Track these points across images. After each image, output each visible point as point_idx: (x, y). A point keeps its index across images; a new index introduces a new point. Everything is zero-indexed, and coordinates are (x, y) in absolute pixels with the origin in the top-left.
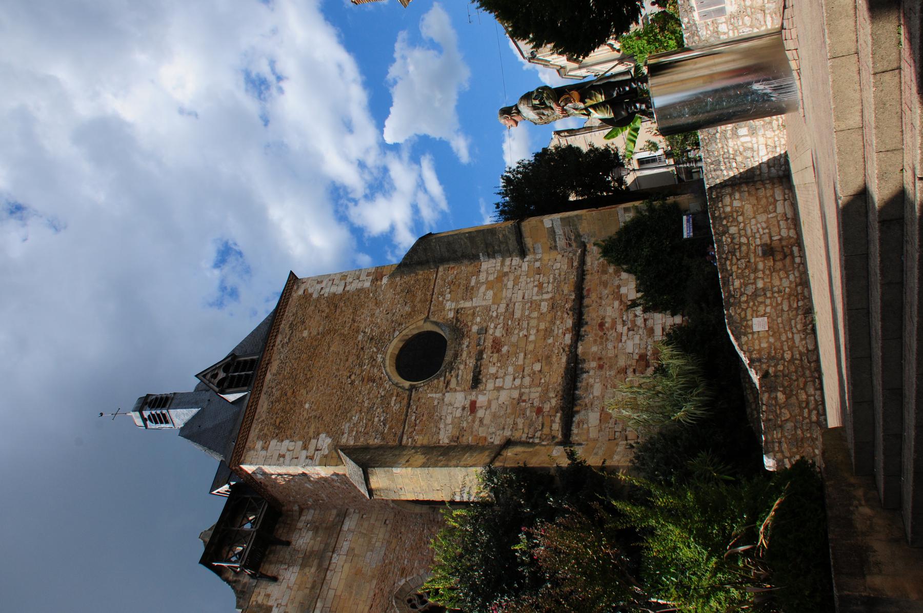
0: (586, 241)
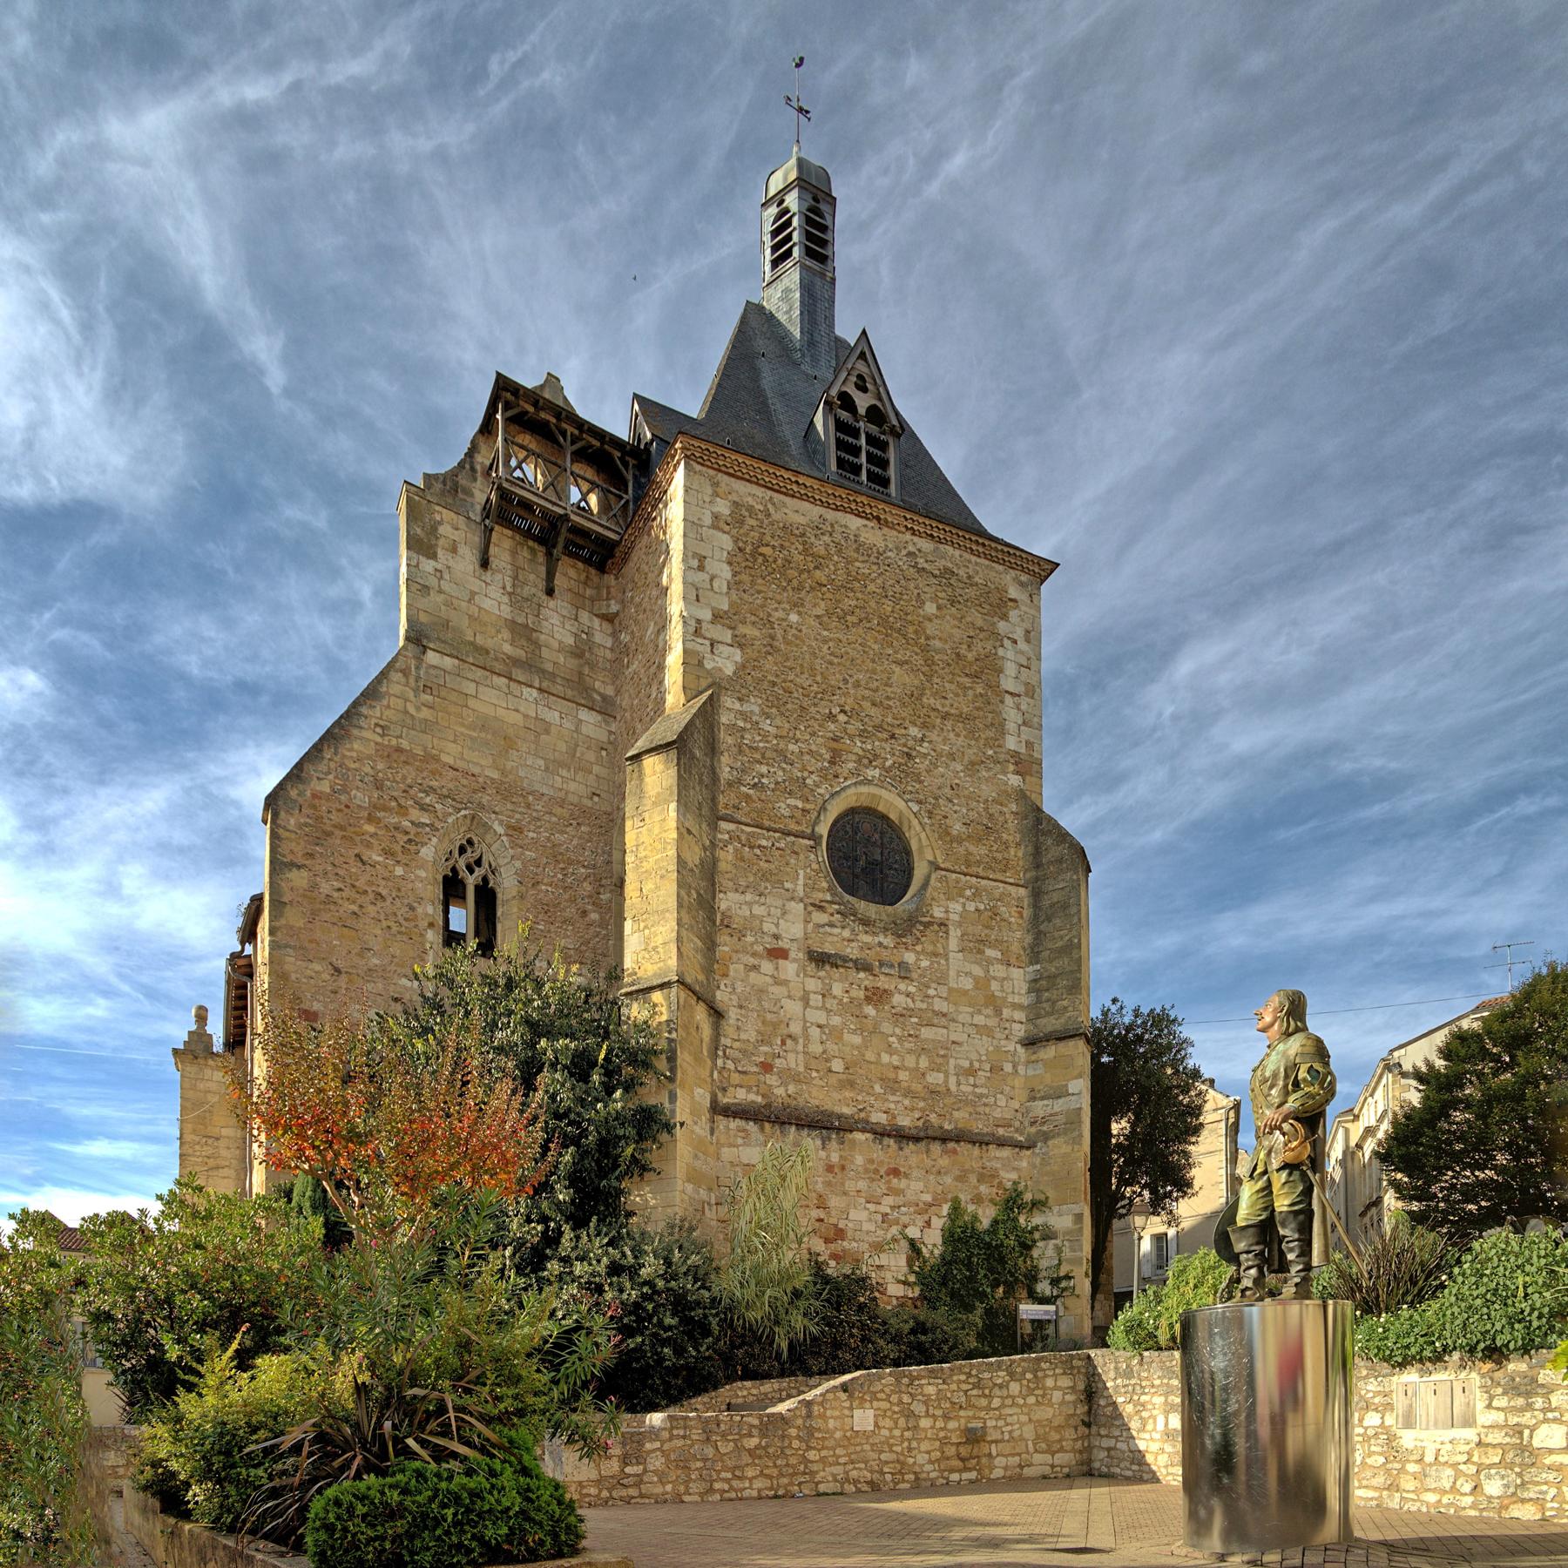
0: (1037, 1150)
